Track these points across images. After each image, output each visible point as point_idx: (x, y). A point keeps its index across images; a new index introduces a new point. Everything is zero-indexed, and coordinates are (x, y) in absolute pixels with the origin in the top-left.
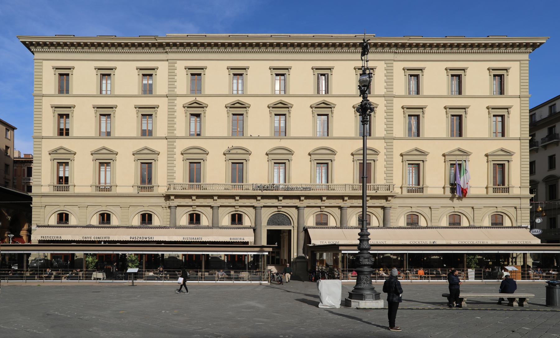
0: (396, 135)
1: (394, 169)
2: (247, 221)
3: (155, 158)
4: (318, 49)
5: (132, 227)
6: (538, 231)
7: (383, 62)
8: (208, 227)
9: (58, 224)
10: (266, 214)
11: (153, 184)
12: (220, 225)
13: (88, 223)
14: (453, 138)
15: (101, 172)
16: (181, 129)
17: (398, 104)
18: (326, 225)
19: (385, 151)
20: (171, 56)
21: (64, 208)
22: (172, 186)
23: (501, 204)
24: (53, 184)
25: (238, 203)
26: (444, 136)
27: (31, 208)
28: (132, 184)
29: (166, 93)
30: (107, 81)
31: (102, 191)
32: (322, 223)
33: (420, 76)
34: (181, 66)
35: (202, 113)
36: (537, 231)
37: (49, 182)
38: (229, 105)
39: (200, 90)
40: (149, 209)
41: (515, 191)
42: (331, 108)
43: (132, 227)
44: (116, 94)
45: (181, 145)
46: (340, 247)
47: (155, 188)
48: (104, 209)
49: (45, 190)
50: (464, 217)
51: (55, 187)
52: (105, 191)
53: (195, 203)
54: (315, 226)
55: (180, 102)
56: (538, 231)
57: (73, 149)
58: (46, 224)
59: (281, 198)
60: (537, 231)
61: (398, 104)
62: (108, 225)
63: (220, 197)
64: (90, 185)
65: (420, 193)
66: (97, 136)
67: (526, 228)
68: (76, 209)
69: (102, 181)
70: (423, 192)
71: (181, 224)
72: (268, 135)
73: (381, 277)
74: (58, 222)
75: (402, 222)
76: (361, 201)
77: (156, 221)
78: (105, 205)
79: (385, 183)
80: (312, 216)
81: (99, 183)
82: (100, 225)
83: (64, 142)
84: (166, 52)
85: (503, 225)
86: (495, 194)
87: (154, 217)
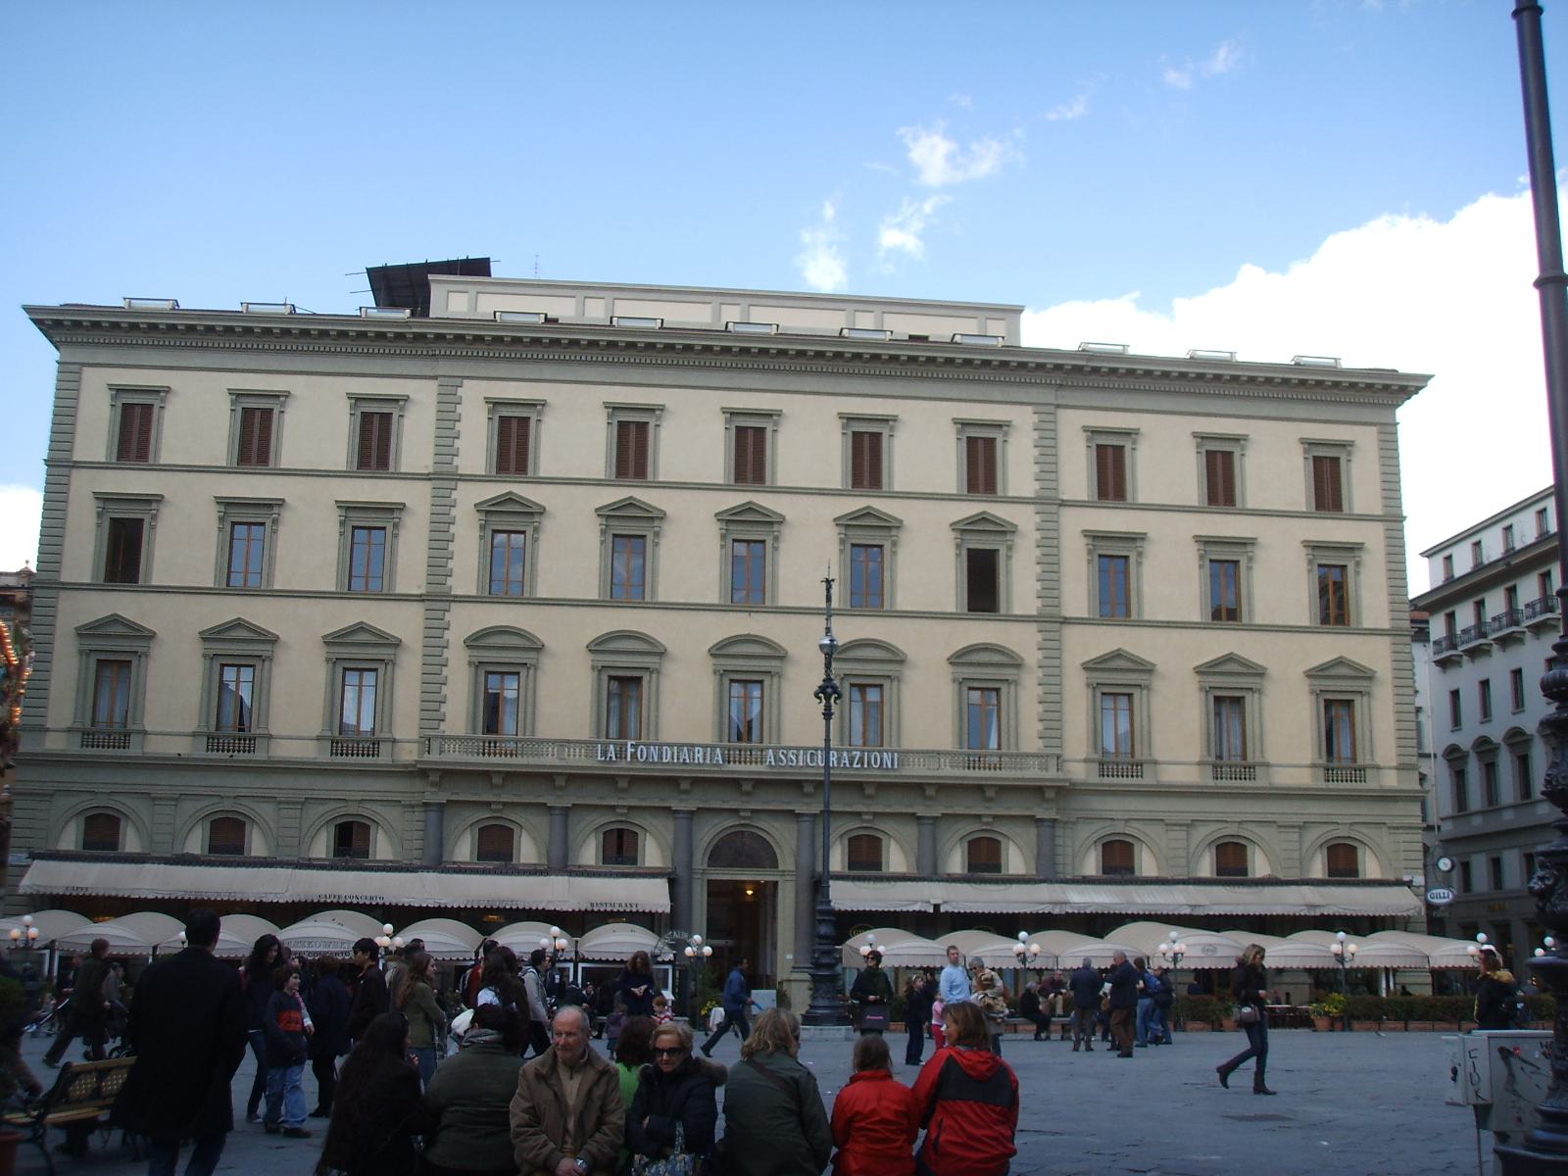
0: (419, 587)
1: (1068, 707)
2: (652, 854)
3: (140, 649)
6: (1446, 895)
7: (1030, 409)
11: (255, 731)
13: (177, 851)
16: (465, 572)
17: (1075, 524)
18: (996, 872)
19: (1040, 655)
20: (444, 368)
21: (1351, 830)
22: (435, 745)
23: (1341, 818)
24: (329, 734)
26: (1196, 618)
28: (193, 727)
29: (426, 467)
31: (1130, 778)
32: (866, 860)
33: (395, 417)
35: (147, 519)
36: (1442, 895)
37: (67, 721)
38: (962, 524)
39: (521, 467)
40: (360, 809)
41: (1390, 780)
44: (899, 490)
45: (465, 621)
46: (223, 920)
47: (1369, 772)
51: (211, 741)
52: (974, 768)
55: (469, 496)
56: (1446, 895)
59: (622, 784)
60: (1442, 895)
61: (1075, 524)
64: (315, 735)
65: (1111, 777)
66: (98, 583)
67: (1409, 884)
68: (1154, 831)
69: (103, 716)
70: (1254, 779)
72: (593, 594)
76: (1416, 809)
77: (382, 847)
78: (1341, 818)
79: (1039, 749)
83: (125, 604)
85: (1246, 874)
87: (889, 846)
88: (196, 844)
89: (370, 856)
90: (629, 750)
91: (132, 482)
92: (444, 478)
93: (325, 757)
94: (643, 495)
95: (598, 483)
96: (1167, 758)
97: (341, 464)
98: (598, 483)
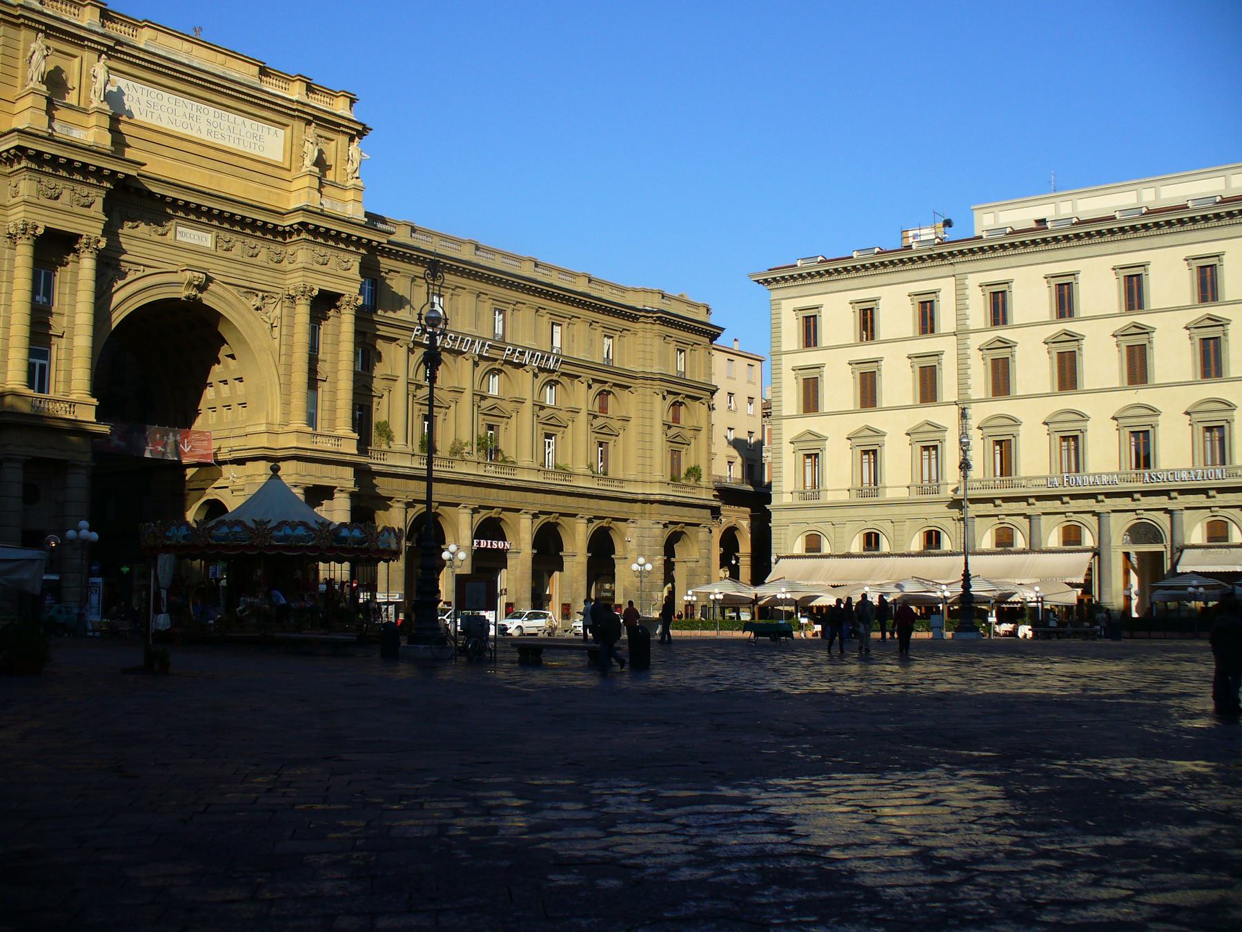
4: (1075, 242)
5: (849, 556)
8: (1023, 552)
9: (864, 550)
10: (1119, 526)
12: (1043, 547)
14: (1132, 312)
15: (807, 468)
20: (960, 268)
25: (1139, 505)
27: (769, 530)
30: (175, 436)
34: (973, 281)
42: (1147, 333)
43: (849, 556)
48: (871, 526)
49: (787, 499)
50: (1234, 525)
53: (1139, 505)
54: (994, 548)
58: (905, 551)
62: (876, 553)
63: (1039, 498)
71: (912, 550)
73: (397, 616)
74: (864, 548)
75: (799, 547)
78: (873, 518)
80: (1199, 525)
81: (805, 486)
82: (865, 553)
83: (1003, 407)
84: (951, 264)
88: (917, 544)
89: (1229, 540)
90: (1065, 480)
91: (811, 357)
92: (961, 333)
93: (915, 497)
94: (1216, 311)
95: (1046, 323)
97: (1187, 301)
98: (1046, 323)
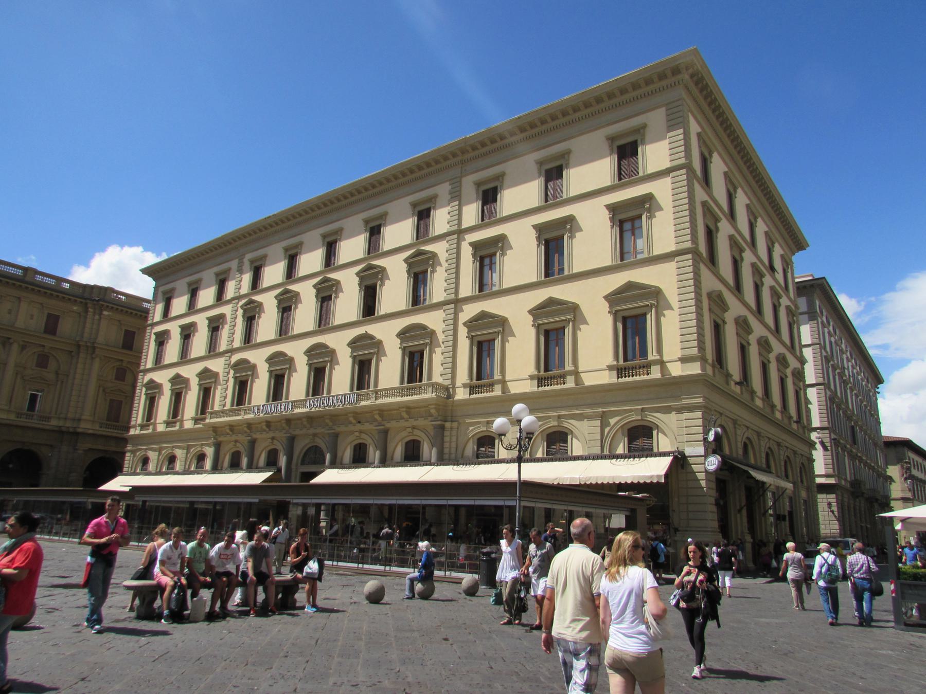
41: (676, 370)
45: (469, 311)
57: (290, 353)
86: (623, 380)
96: (511, 378)
